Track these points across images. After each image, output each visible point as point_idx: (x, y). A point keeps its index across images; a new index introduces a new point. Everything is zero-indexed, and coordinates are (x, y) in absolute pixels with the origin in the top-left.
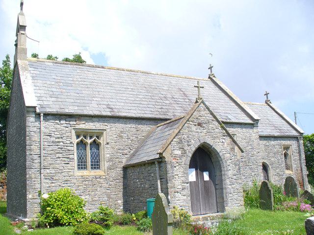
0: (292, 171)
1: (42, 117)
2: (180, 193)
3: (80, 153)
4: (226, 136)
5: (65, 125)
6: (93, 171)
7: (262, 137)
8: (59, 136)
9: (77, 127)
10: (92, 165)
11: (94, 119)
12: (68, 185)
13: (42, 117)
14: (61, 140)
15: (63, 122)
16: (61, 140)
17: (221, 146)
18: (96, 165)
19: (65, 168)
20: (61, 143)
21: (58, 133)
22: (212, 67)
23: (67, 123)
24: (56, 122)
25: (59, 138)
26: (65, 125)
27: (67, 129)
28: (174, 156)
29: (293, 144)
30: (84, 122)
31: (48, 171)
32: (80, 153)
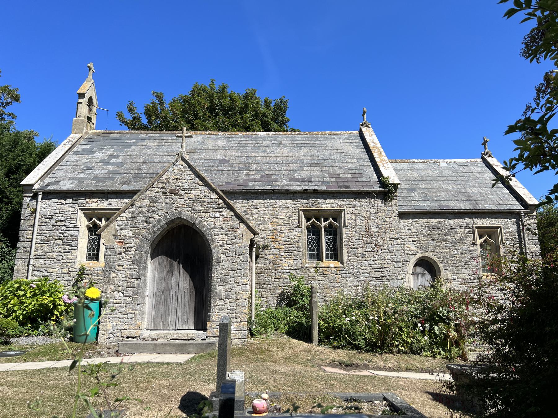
0: (342, 263)
1: (40, 197)
2: (123, 293)
3: (93, 240)
4: (225, 208)
5: (71, 205)
6: (327, 262)
7: (403, 215)
8: (62, 219)
9: (88, 206)
10: (327, 254)
12: (66, 279)
14: (64, 223)
15: (69, 201)
16: (64, 223)
17: (214, 223)
18: (336, 256)
19: (64, 257)
20: (64, 227)
21: (60, 215)
23: (74, 202)
24: (60, 201)
25: (61, 221)
26: (71, 205)
27: (73, 209)
28: (120, 238)
30: (95, 200)
31: (41, 261)
32: (93, 240)
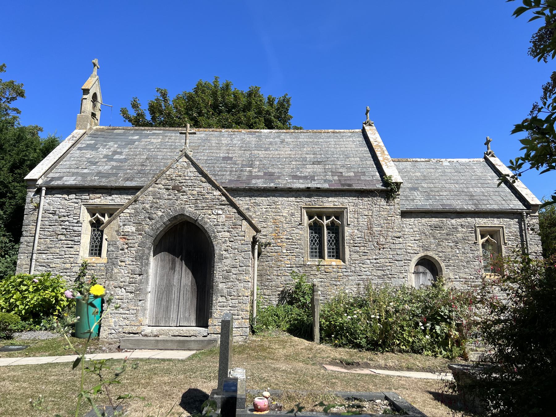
0: (344, 262)
1: (44, 192)
2: (125, 289)
3: (95, 235)
4: (228, 205)
6: (329, 260)
7: (405, 214)
8: (65, 214)
9: (91, 202)
10: (329, 252)
11: (413, 215)
12: (68, 274)
13: (44, 192)
14: (67, 218)
15: (73, 196)
16: (67, 218)
17: (217, 220)
19: (67, 253)
20: (67, 223)
22: (485, 144)
23: (77, 197)
25: (64, 216)
27: (76, 205)
28: (122, 233)
29: (510, 227)
30: (98, 195)
31: (44, 256)
